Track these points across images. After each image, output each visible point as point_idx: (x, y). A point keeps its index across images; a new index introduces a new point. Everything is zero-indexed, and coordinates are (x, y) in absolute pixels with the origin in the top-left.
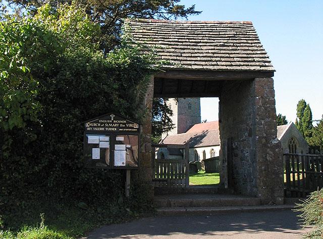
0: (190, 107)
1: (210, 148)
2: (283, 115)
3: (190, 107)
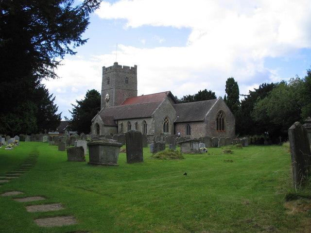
0: (127, 82)
1: (135, 121)
2: (213, 92)
3: (127, 82)
